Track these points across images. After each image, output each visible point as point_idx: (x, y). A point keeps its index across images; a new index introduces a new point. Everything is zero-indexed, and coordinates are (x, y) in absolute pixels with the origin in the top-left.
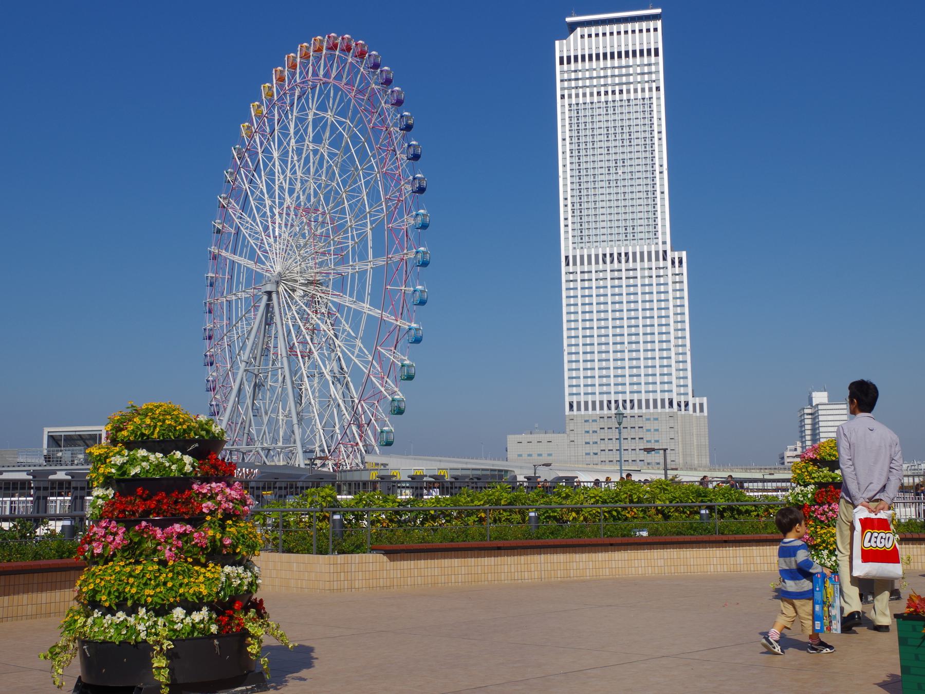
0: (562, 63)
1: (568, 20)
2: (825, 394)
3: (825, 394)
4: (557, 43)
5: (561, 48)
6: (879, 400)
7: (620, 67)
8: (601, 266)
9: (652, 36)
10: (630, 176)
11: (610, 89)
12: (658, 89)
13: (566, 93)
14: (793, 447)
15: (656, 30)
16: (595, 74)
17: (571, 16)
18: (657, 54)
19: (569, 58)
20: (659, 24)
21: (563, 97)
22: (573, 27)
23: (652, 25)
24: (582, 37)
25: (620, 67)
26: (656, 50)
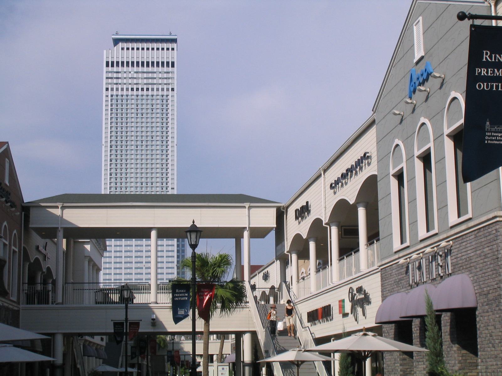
0: (107, 65)
13: (110, 87)
24: (123, 49)
25: (168, 73)
26: (173, 64)
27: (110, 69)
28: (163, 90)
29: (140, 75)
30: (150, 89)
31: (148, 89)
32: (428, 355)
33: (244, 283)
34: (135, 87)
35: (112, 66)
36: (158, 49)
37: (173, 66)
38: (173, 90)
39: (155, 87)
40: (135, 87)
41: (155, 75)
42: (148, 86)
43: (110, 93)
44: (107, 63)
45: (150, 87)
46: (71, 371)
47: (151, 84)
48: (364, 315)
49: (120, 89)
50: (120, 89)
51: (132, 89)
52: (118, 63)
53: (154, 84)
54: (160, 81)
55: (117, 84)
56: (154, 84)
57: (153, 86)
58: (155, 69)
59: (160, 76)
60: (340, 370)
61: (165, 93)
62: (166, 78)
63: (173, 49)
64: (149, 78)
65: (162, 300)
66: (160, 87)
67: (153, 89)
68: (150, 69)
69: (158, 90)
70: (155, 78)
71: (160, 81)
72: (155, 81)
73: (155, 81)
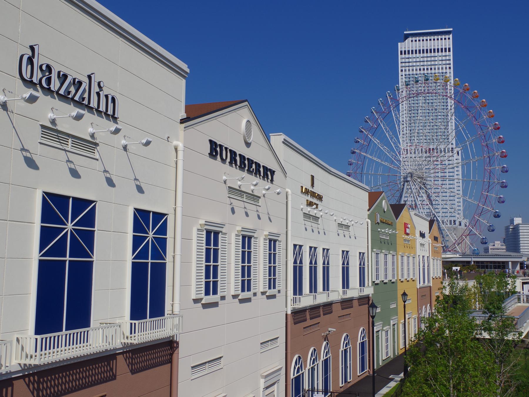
0: (401, 54)
1: (405, 32)
2: (520, 219)
3: (520, 219)
4: (399, 44)
5: (401, 46)
6: (26, 165)
7: (446, 56)
8: (420, 155)
9: (448, 42)
10: (413, 109)
11: (426, 68)
12: (450, 68)
13: (403, 69)
14: (493, 244)
15: (449, 39)
16: (418, 60)
17: (406, 31)
18: (449, 51)
19: (405, 51)
20: (451, 36)
21: (402, 71)
22: (407, 37)
23: (447, 37)
24: (412, 41)
25: (446, 56)
26: (449, 49)
27: (403, 56)
28: (442, 68)
29: (425, 59)
31: (431, 69)
34: (422, 68)
35: (405, 54)
36: (434, 40)
40: (422, 68)
41: (436, 59)
43: (404, 73)
45: (433, 67)
47: (404, 67)
48: (40, 143)
49: (437, 69)
50: (437, 69)
51: (420, 70)
52: (416, 51)
53: (414, 66)
55: (423, 66)
56: (414, 66)
57: (435, 66)
61: (444, 71)
62: (430, 61)
64: (432, 61)
65: (524, 248)
66: (440, 67)
67: (435, 69)
68: (407, 56)
69: (439, 69)
70: (436, 61)
72: (436, 63)
73: (436, 63)
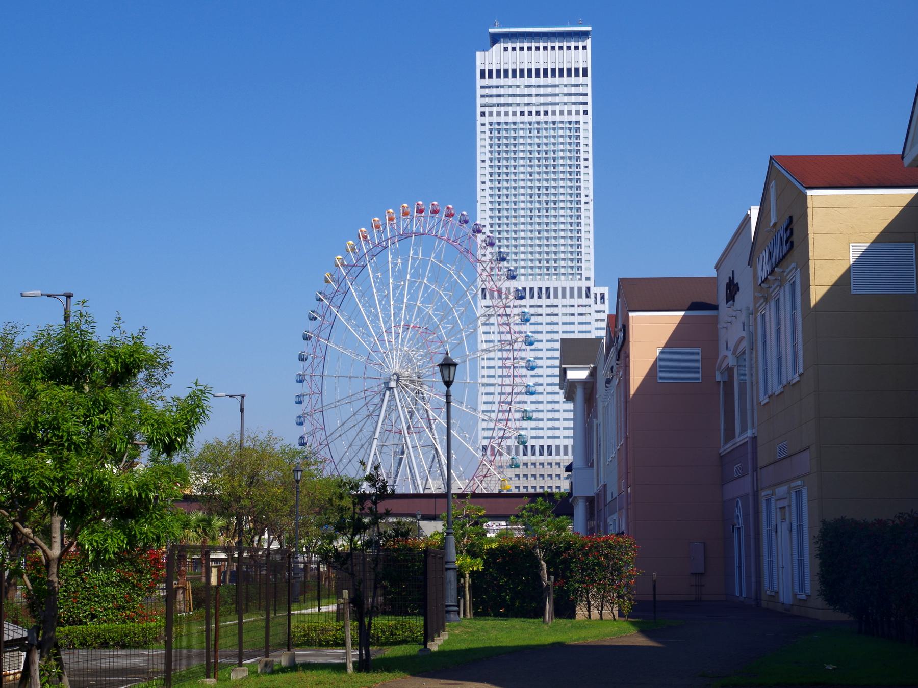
0: (482, 76)
24: (506, 49)
26: (585, 71)
28: (570, 113)
30: (550, 113)
31: (546, 113)
32: (405, 535)
33: (193, 411)
37: (585, 75)
38: (585, 112)
39: (558, 108)
42: (538, 108)
44: (482, 73)
45: (550, 109)
46: (770, 553)
54: (566, 99)
57: (554, 108)
58: (502, 81)
59: (566, 90)
60: (817, 570)
61: (574, 118)
63: (585, 48)
66: (566, 108)
67: (554, 113)
71: (566, 99)
